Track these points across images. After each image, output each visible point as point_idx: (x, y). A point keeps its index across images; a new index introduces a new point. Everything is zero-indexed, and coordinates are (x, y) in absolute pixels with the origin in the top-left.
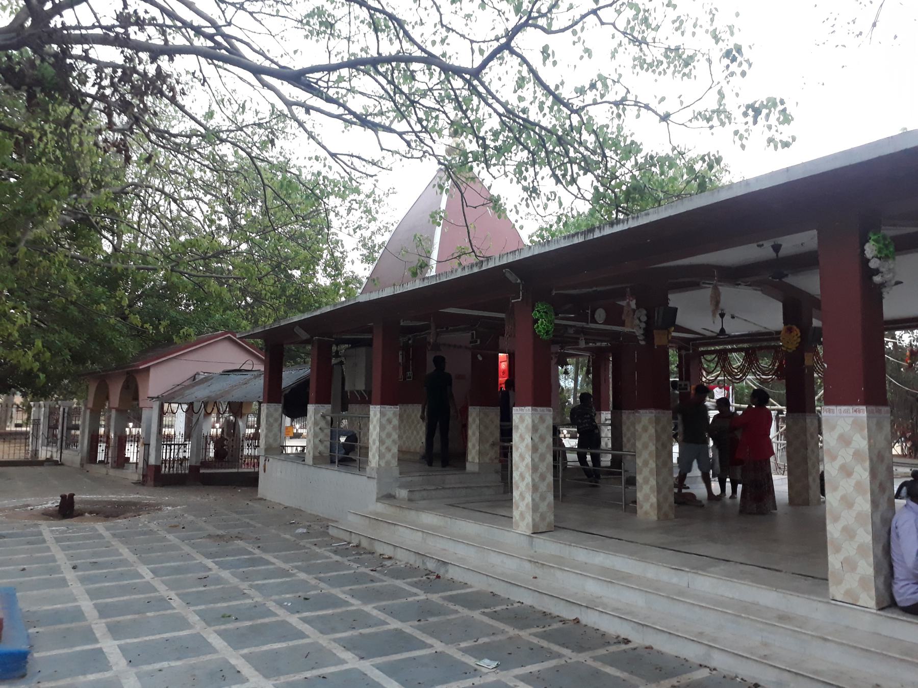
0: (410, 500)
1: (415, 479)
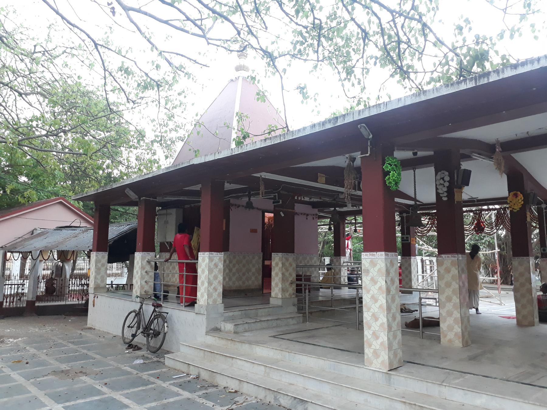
0: (235, 333)
1: (236, 313)
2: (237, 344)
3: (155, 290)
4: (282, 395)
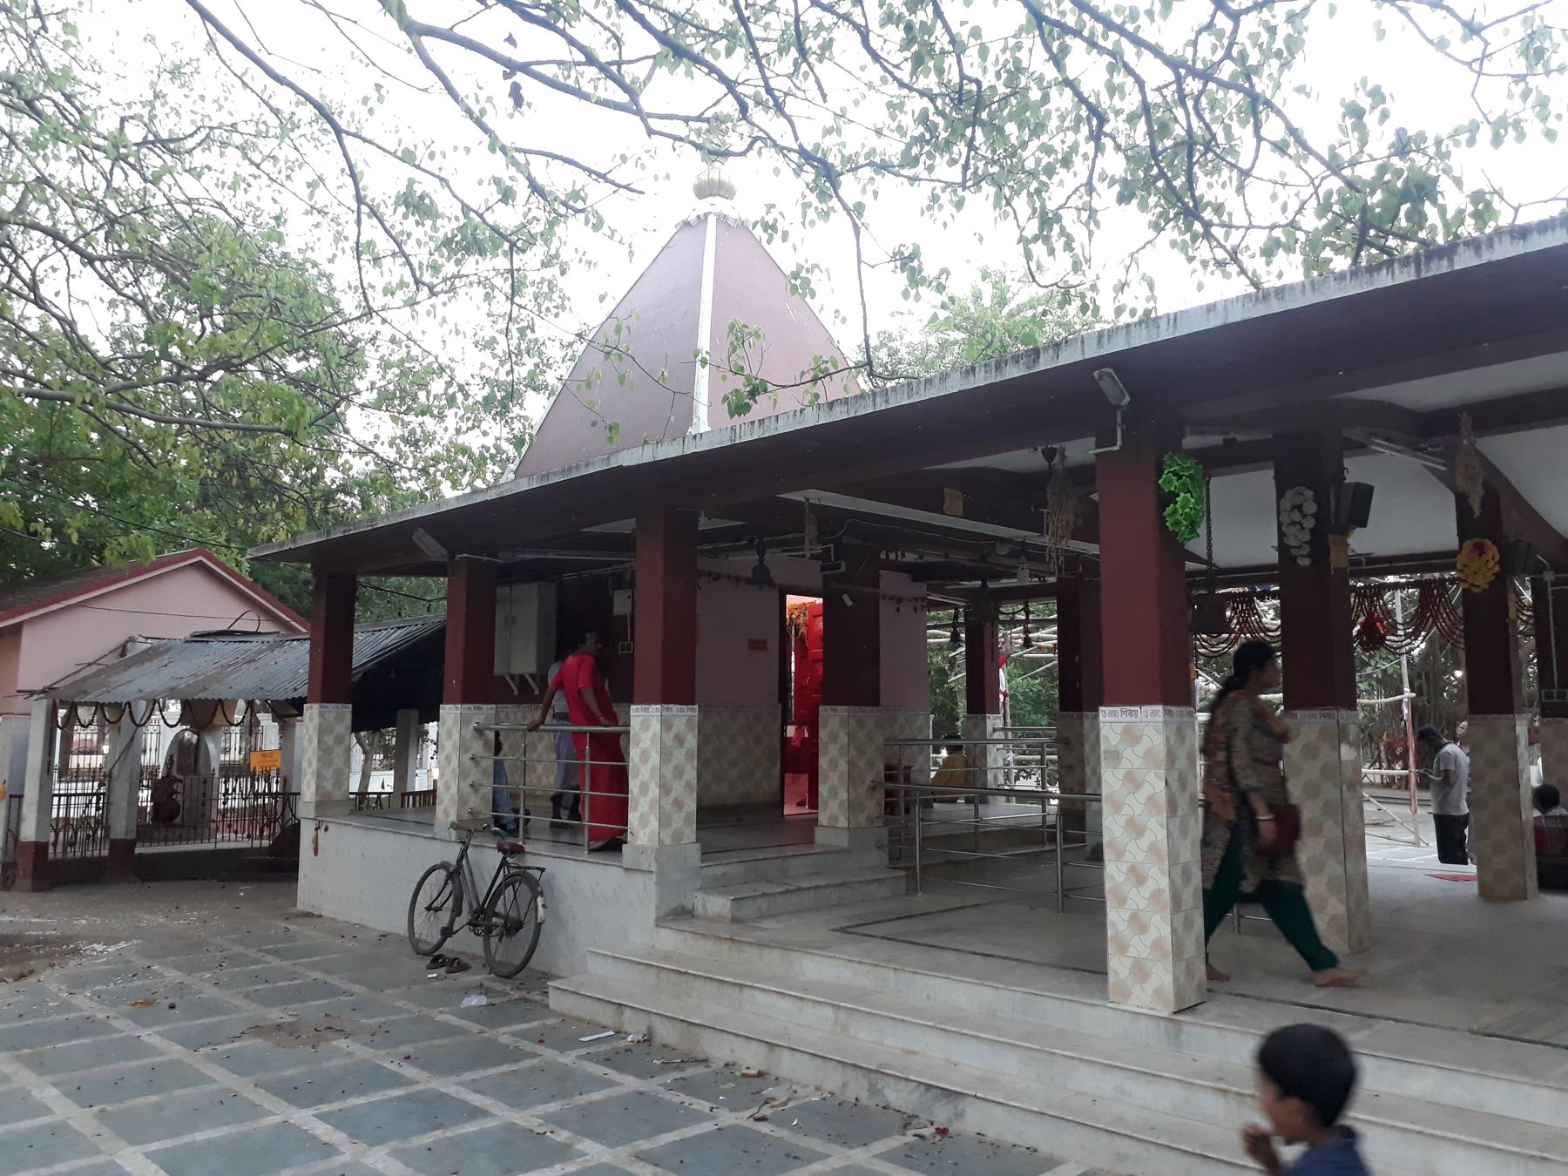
0: (735, 920)
1: (732, 869)
2: (747, 948)
3: (495, 808)
4: (892, 1081)
